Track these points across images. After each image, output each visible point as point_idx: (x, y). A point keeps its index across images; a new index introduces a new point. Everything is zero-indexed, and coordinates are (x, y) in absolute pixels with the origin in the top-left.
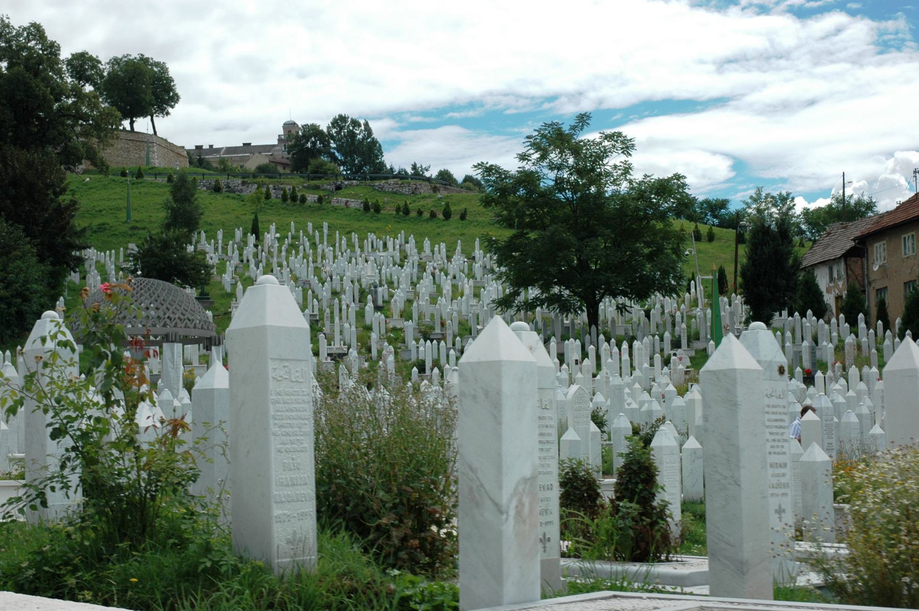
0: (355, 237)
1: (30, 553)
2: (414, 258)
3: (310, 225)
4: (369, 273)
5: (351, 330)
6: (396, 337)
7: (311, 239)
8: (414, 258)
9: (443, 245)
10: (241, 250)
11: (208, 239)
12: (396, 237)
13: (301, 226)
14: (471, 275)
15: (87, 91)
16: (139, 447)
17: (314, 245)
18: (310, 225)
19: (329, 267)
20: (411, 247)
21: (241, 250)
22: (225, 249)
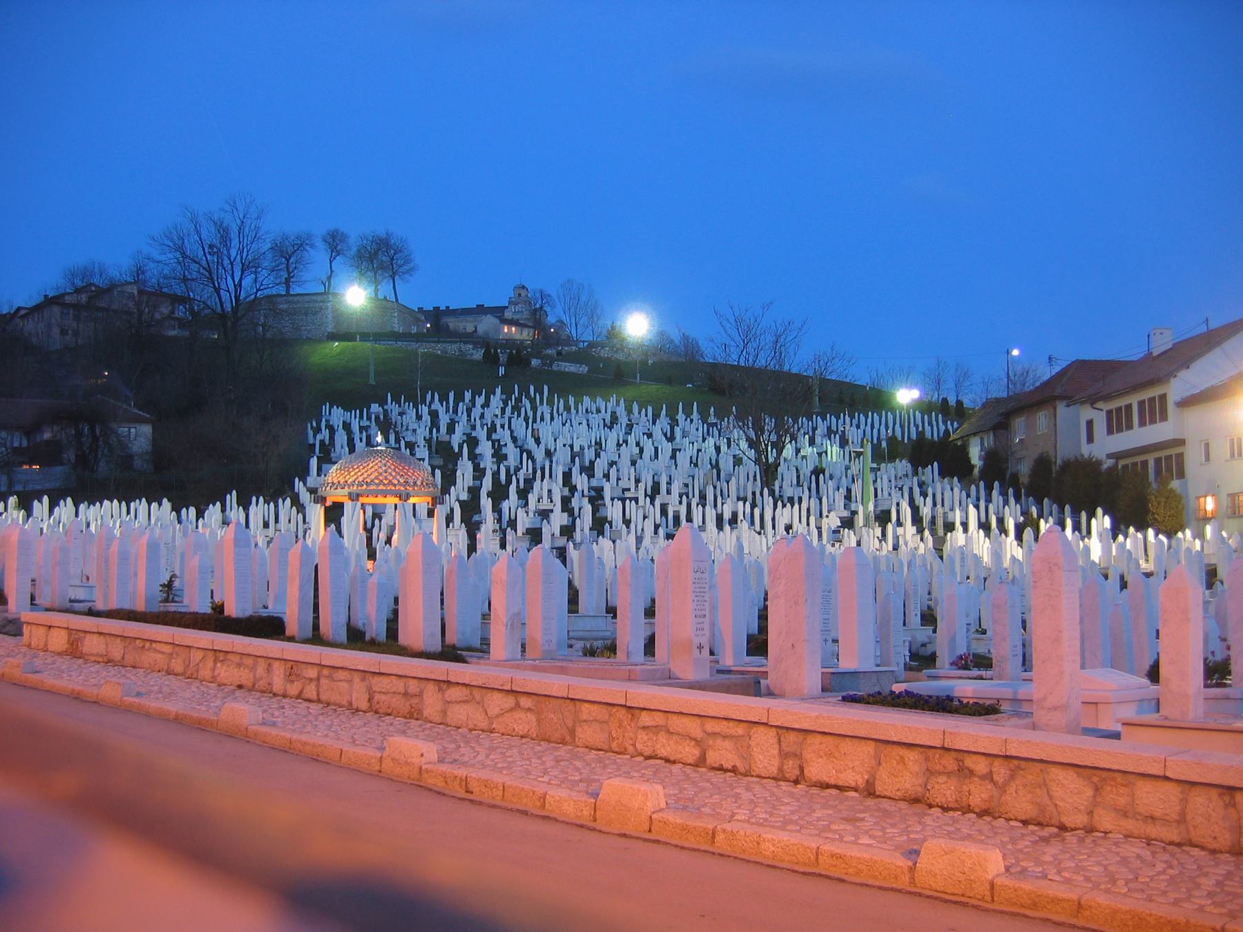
0: (571, 400)
1: (1230, 686)
2: (624, 420)
3: (532, 388)
4: (582, 437)
5: (558, 491)
6: (596, 497)
7: (533, 401)
8: (624, 420)
9: (650, 409)
10: (469, 411)
11: (441, 402)
12: (607, 401)
13: (524, 390)
14: (671, 439)
15: (147, 429)
16: (1042, 464)
17: (534, 409)
18: (532, 388)
19: (546, 431)
20: (621, 411)
21: (469, 411)
22: (456, 411)
